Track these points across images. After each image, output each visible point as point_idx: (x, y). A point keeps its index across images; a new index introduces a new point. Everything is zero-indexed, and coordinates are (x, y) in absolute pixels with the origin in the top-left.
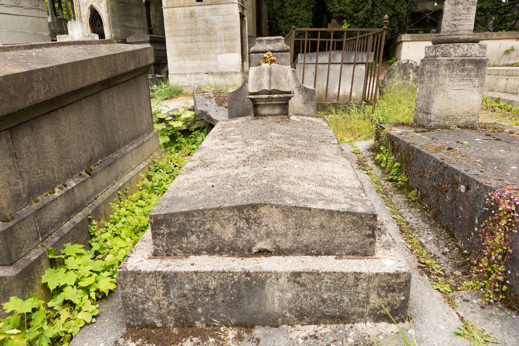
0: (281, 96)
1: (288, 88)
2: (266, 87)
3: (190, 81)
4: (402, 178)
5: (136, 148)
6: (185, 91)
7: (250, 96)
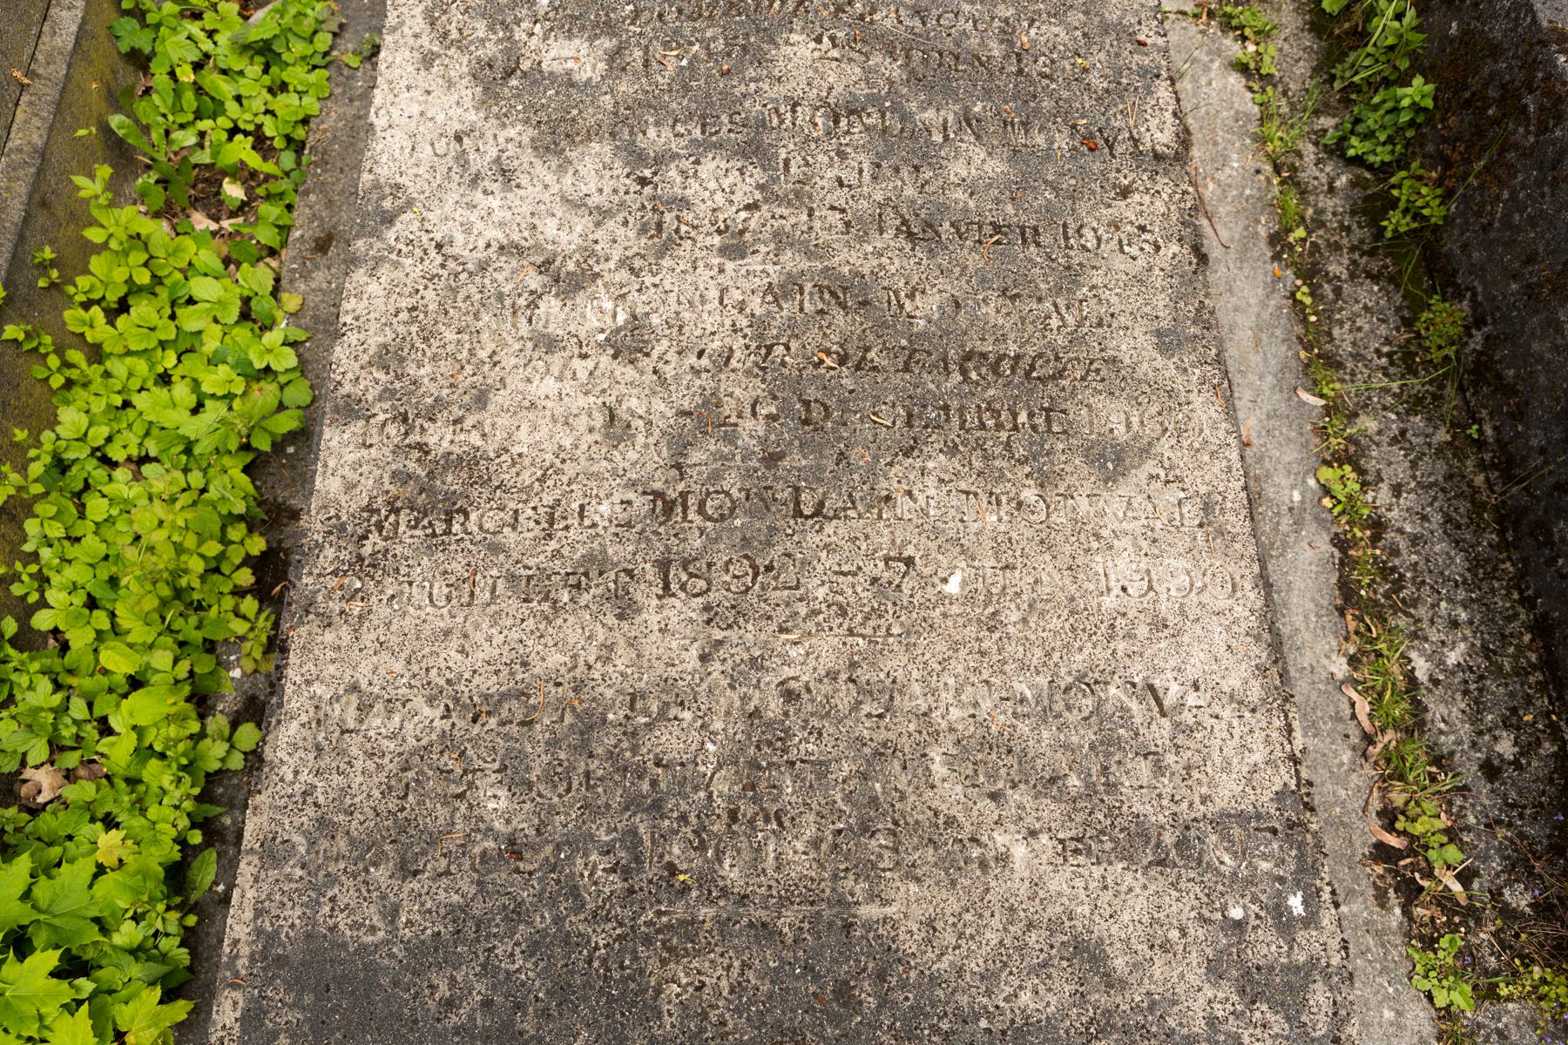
4: (1417, 193)
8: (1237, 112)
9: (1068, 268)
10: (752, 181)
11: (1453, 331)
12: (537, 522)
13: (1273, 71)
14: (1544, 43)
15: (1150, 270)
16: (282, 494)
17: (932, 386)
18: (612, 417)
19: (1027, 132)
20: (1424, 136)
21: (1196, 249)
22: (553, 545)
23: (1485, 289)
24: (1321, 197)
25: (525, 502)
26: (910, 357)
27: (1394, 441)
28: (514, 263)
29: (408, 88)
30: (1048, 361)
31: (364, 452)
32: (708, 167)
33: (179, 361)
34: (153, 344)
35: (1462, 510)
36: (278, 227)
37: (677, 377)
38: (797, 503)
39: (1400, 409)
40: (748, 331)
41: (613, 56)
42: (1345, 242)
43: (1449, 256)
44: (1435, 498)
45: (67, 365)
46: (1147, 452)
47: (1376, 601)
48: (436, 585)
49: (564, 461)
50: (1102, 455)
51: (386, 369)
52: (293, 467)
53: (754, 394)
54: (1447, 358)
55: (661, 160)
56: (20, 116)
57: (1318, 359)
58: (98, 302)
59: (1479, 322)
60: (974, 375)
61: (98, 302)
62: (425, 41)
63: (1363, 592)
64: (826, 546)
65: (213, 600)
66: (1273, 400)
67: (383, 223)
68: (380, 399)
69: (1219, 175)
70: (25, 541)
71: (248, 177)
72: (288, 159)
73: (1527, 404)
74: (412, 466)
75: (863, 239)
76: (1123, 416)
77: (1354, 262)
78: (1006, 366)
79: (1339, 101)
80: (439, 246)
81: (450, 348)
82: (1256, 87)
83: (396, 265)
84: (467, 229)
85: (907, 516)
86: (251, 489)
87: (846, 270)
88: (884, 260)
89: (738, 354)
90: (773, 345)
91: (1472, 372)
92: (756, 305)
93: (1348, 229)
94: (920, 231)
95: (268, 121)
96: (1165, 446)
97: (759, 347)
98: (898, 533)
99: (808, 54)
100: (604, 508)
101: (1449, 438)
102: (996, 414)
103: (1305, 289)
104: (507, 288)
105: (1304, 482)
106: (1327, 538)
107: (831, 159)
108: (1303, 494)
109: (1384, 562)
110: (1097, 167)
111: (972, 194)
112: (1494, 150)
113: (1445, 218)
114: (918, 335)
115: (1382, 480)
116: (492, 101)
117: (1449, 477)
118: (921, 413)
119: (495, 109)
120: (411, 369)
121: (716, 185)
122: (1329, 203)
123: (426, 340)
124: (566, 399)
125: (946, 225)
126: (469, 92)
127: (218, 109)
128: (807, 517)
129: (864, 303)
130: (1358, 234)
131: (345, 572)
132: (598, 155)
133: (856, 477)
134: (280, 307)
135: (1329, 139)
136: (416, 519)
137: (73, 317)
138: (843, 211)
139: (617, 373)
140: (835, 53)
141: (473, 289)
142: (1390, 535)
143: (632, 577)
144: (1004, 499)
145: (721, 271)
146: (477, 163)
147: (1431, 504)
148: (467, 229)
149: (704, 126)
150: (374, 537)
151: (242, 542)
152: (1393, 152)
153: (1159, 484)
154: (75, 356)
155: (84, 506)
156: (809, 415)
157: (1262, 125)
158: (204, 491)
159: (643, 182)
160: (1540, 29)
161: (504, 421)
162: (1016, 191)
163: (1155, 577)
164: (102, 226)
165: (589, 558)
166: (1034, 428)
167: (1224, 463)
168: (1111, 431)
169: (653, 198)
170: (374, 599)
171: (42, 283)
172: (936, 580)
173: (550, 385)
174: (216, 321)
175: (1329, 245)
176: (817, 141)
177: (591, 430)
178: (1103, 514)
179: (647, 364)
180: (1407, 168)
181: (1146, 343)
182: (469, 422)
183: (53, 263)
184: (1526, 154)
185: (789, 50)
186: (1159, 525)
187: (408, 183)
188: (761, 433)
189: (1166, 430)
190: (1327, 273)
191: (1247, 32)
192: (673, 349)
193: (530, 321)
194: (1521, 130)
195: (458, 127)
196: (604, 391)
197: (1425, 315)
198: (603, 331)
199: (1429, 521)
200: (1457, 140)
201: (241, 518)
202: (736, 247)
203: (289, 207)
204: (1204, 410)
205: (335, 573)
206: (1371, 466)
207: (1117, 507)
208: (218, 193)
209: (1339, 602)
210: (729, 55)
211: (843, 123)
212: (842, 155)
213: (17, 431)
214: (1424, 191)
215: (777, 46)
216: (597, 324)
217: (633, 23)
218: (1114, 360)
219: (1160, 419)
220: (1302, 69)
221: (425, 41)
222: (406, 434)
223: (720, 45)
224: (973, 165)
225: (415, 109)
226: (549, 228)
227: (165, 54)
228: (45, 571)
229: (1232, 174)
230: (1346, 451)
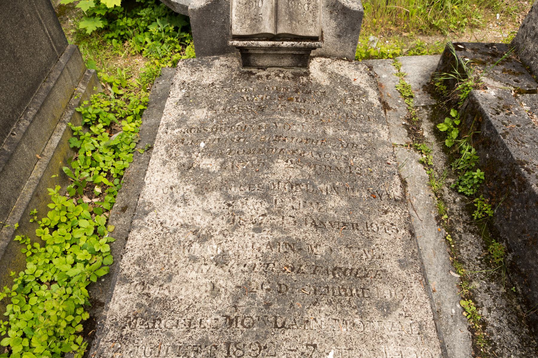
1: (312, 29)
2: (267, 28)
4: (483, 206)
5: (34, 118)
7: (236, 43)
8: (422, 176)
9: (368, 238)
10: (264, 206)
11: (501, 253)
12: (185, 325)
13: (432, 164)
14: (517, 165)
15: (395, 239)
16: (98, 296)
17: (323, 280)
18: (214, 287)
19: (353, 192)
20: (482, 187)
21: (410, 232)
22: (190, 334)
23: (510, 239)
24: (452, 205)
25: (181, 317)
26: (315, 269)
27: (486, 291)
28: (185, 231)
29: (157, 171)
30: (362, 271)
31: (128, 295)
32: (251, 201)
33: (71, 246)
34: (63, 241)
35: (514, 319)
36: (110, 203)
37: (236, 273)
38: (276, 322)
39: (487, 279)
40: (261, 258)
41: (222, 164)
42: (461, 220)
43: (496, 227)
44: (503, 314)
45: (34, 248)
46: (398, 305)
47: (487, 354)
48: (147, 348)
49: (196, 303)
50: (382, 306)
51: (139, 265)
52: (103, 286)
53: (262, 281)
54: (500, 262)
55: (235, 198)
56: (36, 168)
57: (456, 261)
58: (48, 226)
59: (510, 251)
60: (337, 276)
61: (48, 226)
62: (164, 157)
63: (482, 350)
64: (286, 339)
65: (67, 336)
66: (442, 275)
67: (144, 215)
68: (136, 276)
69: (417, 196)
70: (6, 311)
71: (103, 186)
72: (117, 181)
73: (531, 282)
74: (144, 301)
75: (300, 227)
76: (389, 291)
77: (465, 227)
78: (348, 272)
79: (454, 174)
80: (161, 223)
81: (161, 259)
82: (427, 169)
83: (147, 229)
84: (171, 218)
85: (314, 328)
86: (87, 294)
87: (294, 237)
88: (307, 234)
89: (257, 266)
90: (269, 264)
91: (510, 268)
92: (264, 249)
93: (462, 216)
94: (319, 225)
95: (112, 169)
96: (404, 303)
97: (264, 264)
98: (311, 335)
99: (283, 166)
100: (209, 321)
101: (505, 291)
102: (345, 290)
103: (449, 236)
104: (182, 239)
105: (456, 306)
106: (466, 328)
107: (290, 200)
108: (455, 310)
109: (488, 338)
110: (376, 203)
111: (336, 212)
112: (506, 195)
113: (493, 214)
114: (319, 261)
115: (484, 306)
116: (183, 177)
117: (507, 306)
118: (319, 289)
119: (184, 179)
120: (148, 266)
121: (253, 208)
122: (454, 207)
123: (154, 256)
124: (199, 280)
125: (328, 222)
126: (176, 173)
127: (98, 164)
128: (279, 328)
129: (300, 249)
130: (465, 217)
131: (116, 341)
132: (215, 196)
133: (296, 313)
134: (107, 230)
135: (453, 186)
136: (143, 322)
137: (38, 232)
138: (294, 217)
139: (217, 271)
140: (292, 166)
141: (171, 239)
142: (489, 327)
143: (216, 349)
144: (348, 322)
145: (253, 237)
146: (177, 196)
147: (502, 316)
148: (171, 218)
149: (250, 188)
150: (127, 328)
151: (81, 315)
152: (473, 191)
153: (403, 318)
154: (37, 245)
155: (29, 299)
156: (281, 290)
157: (430, 181)
158: (71, 295)
159: (229, 205)
160: (514, 160)
161: (177, 286)
162: (350, 211)
163: (403, 354)
164: (54, 203)
165: (202, 340)
166: (358, 295)
167: (425, 310)
168: (385, 297)
169: (232, 211)
170: (124, 352)
171: (31, 221)
172: (324, 354)
173: (193, 274)
174: (85, 235)
175: (456, 221)
176: (286, 194)
177: (206, 291)
178: (383, 329)
179: (227, 268)
180: (478, 197)
181: (396, 265)
182: (165, 286)
183: (36, 214)
184: (517, 197)
185: (277, 165)
186: (404, 333)
187: (154, 202)
188: (264, 296)
189: (404, 297)
190: (456, 230)
191: (423, 151)
192: (236, 263)
193: (189, 251)
194: (514, 190)
195: (172, 184)
196: (211, 277)
197: (491, 247)
198: (213, 256)
199: (502, 322)
200: (493, 190)
201: (82, 306)
202: (258, 229)
203: (115, 197)
204: (417, 289)
205: (112, 341)
206: (479, 300)
207: (388, 326)
208: (93, 190)
209: (473, 353)
210: (259, 165)
211: (294, 188)
212: (294, 199)
213: (12, 272)
214: (485, 205)
215: (274, 163)
216: (211, 253)
217: (229, 154)
218: (385, 271)
219: (402, 293)
220: (441, 163)
221: (164, 157)
222: (143, 289)
223: (256, 162)
224: (336, 202)
225: (159, 178)
226: (198, 219)
227: (84, 148)
228: (10, 323)
229: (421, 196)
230: (469, 294)
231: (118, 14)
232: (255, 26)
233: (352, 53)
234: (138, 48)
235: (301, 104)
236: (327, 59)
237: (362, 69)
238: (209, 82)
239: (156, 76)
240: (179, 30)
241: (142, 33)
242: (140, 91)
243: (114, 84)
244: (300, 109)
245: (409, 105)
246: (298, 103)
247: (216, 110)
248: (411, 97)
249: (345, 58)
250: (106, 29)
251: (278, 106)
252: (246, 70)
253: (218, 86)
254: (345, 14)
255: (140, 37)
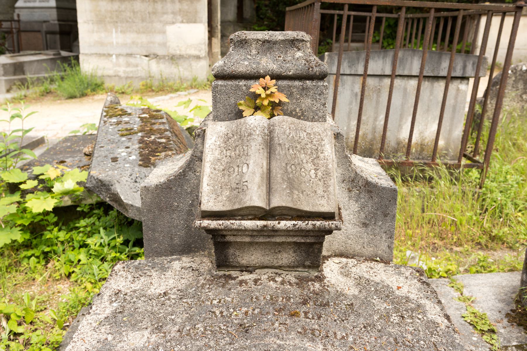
0: (301, 224)
1: (323, 202)
2: (256, 198)
3: (117, 68)
6: (108, 84)
7: (206, 223)
231: (48, 225)
232: (236, 198)
233: (388, 250)
234: (65, 270)
235: (313, 321)
236: (350, 260)
237: (408, 274)
238: (161, 290)
239: (84, 304)
240: (131, 244)
241: (76, 250)
242: (53, 328)
243: (12, 316)
244: (313, 330)
245: (492, 345)
246: (308, 320)
247: (165, 333)
248: (493, 331)
249: (378, 259)
250: (27, 245)
251: (273, 324)
252: (221, 273)
253: (173, 297)
254: (370, 192)
255: (72, 255)
